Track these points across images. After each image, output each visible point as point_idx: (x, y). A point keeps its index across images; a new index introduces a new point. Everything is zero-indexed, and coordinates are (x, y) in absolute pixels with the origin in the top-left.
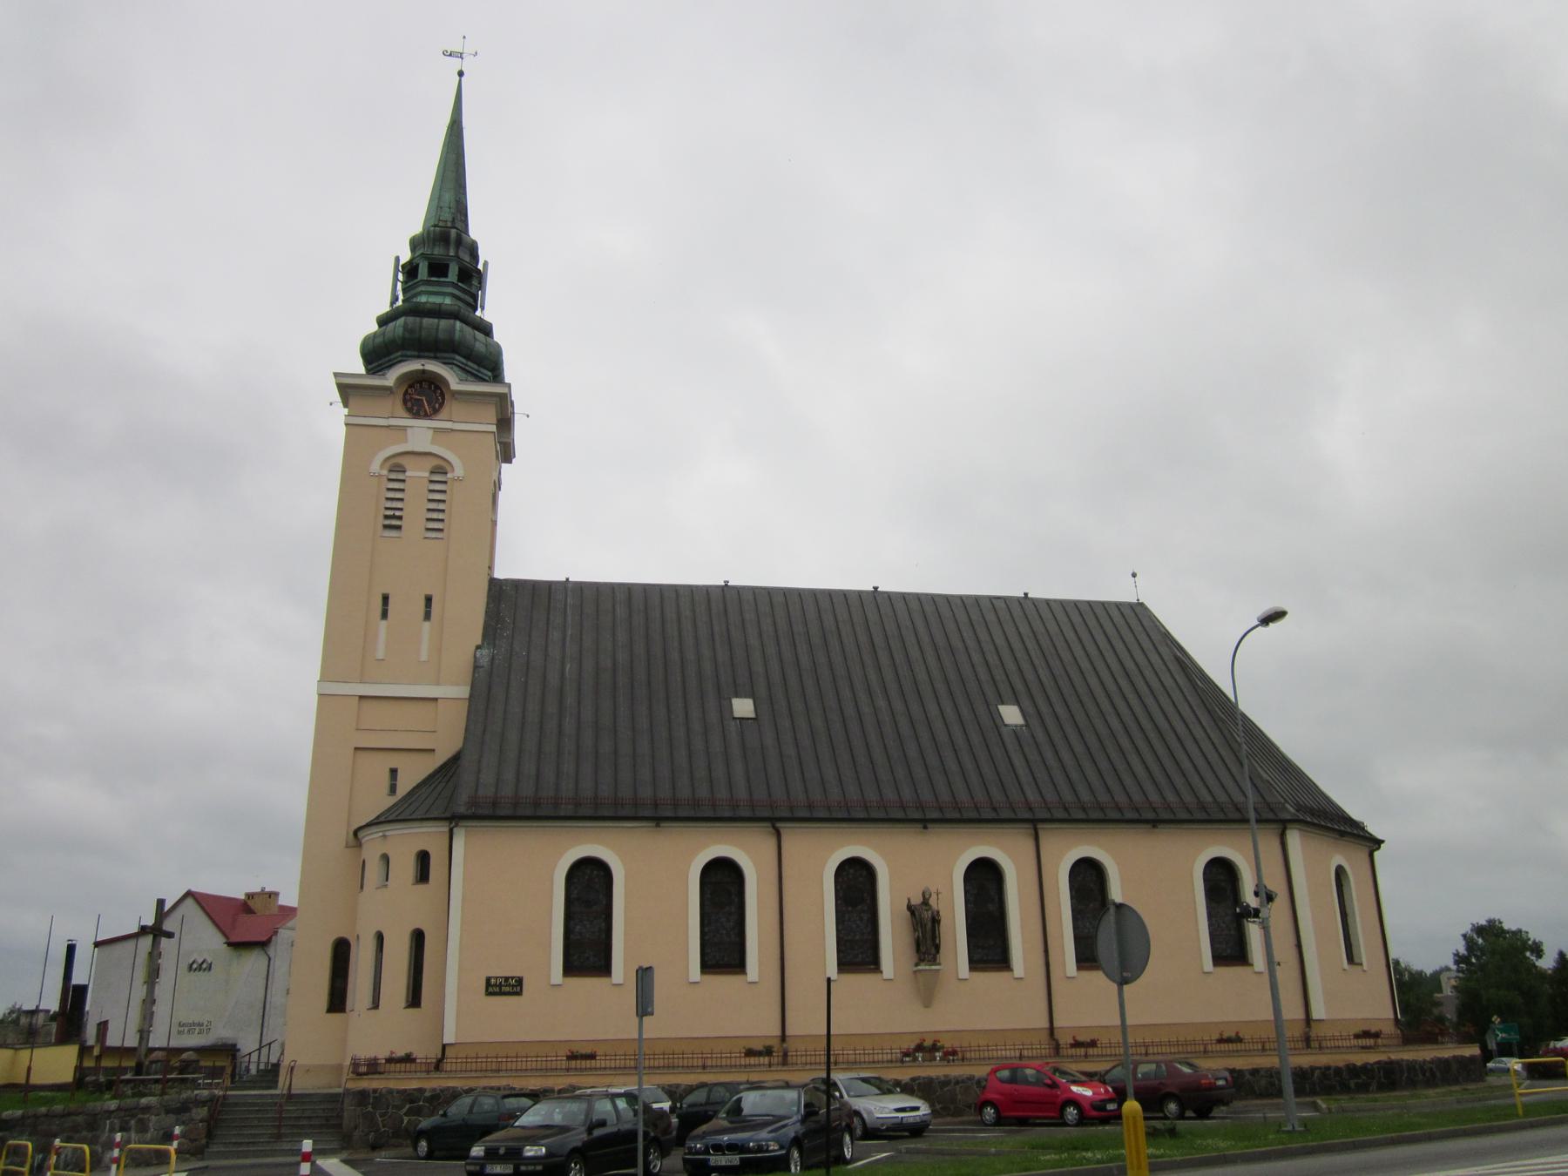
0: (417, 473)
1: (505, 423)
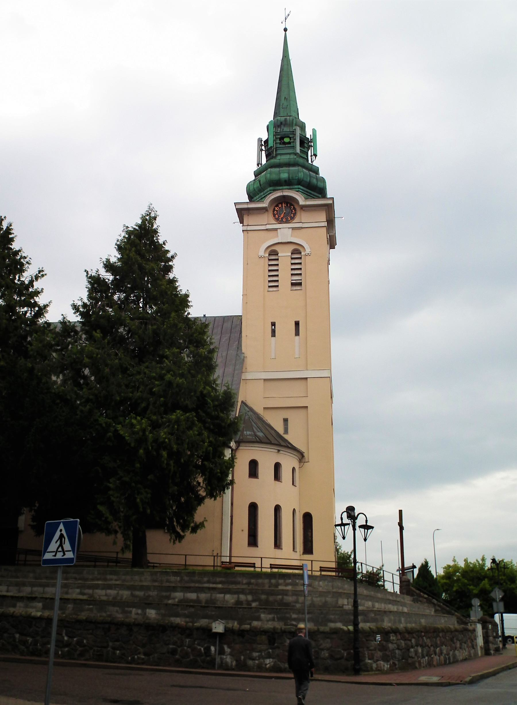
0: (285, 253)
1: (331, 222)
